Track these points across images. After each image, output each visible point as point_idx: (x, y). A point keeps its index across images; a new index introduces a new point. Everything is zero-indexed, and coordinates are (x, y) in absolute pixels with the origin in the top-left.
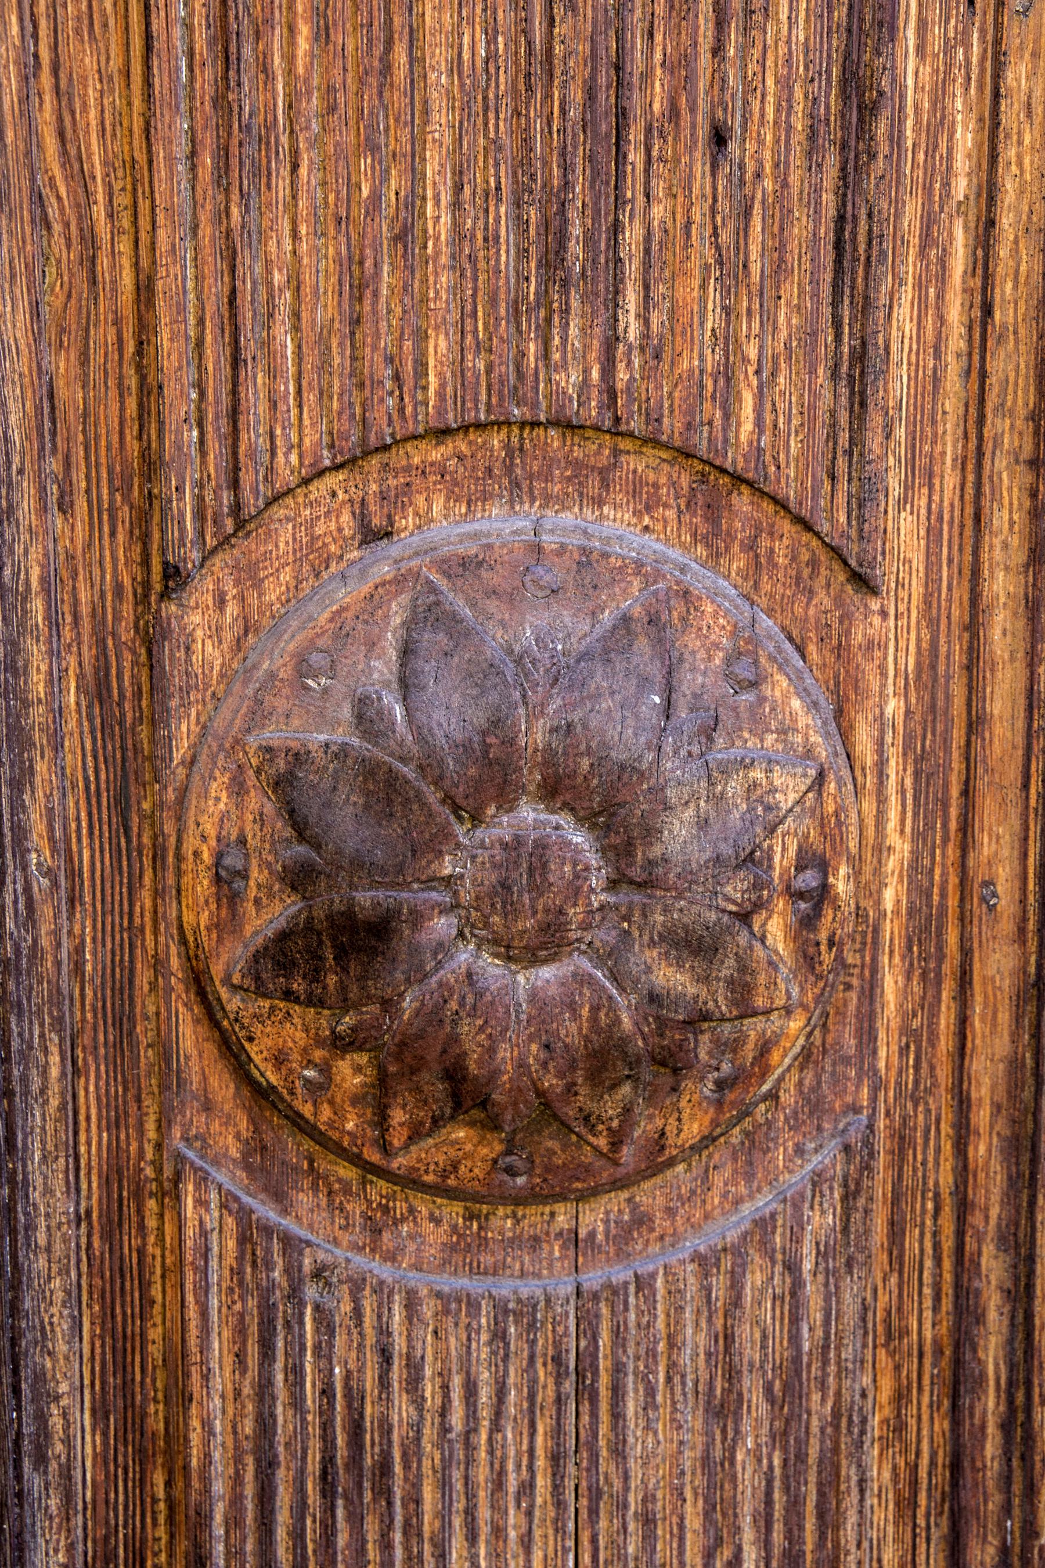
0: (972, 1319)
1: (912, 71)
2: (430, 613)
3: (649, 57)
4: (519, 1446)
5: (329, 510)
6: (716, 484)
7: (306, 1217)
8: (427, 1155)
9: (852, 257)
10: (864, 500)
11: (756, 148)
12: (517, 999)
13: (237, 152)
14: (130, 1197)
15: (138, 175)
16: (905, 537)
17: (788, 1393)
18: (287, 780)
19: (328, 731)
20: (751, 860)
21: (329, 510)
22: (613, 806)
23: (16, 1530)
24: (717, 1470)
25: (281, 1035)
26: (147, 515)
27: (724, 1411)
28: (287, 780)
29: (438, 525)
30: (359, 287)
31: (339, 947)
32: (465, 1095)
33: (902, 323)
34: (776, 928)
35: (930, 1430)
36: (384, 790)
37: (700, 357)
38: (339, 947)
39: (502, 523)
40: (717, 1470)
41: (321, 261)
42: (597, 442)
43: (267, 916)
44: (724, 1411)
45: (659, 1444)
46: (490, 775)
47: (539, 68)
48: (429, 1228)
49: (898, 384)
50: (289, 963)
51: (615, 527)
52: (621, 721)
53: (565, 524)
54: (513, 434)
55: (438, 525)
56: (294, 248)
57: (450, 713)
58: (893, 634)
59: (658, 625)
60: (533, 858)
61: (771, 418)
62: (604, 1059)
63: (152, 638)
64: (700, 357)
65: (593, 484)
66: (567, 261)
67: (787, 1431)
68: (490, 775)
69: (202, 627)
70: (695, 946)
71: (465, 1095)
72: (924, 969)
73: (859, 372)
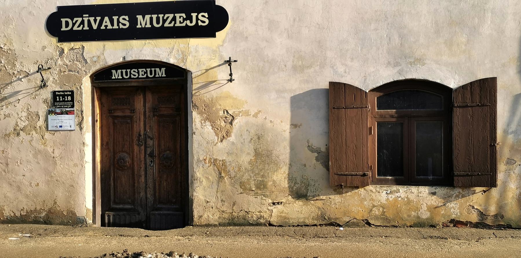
6: (127, 153)
46: (120, 159)
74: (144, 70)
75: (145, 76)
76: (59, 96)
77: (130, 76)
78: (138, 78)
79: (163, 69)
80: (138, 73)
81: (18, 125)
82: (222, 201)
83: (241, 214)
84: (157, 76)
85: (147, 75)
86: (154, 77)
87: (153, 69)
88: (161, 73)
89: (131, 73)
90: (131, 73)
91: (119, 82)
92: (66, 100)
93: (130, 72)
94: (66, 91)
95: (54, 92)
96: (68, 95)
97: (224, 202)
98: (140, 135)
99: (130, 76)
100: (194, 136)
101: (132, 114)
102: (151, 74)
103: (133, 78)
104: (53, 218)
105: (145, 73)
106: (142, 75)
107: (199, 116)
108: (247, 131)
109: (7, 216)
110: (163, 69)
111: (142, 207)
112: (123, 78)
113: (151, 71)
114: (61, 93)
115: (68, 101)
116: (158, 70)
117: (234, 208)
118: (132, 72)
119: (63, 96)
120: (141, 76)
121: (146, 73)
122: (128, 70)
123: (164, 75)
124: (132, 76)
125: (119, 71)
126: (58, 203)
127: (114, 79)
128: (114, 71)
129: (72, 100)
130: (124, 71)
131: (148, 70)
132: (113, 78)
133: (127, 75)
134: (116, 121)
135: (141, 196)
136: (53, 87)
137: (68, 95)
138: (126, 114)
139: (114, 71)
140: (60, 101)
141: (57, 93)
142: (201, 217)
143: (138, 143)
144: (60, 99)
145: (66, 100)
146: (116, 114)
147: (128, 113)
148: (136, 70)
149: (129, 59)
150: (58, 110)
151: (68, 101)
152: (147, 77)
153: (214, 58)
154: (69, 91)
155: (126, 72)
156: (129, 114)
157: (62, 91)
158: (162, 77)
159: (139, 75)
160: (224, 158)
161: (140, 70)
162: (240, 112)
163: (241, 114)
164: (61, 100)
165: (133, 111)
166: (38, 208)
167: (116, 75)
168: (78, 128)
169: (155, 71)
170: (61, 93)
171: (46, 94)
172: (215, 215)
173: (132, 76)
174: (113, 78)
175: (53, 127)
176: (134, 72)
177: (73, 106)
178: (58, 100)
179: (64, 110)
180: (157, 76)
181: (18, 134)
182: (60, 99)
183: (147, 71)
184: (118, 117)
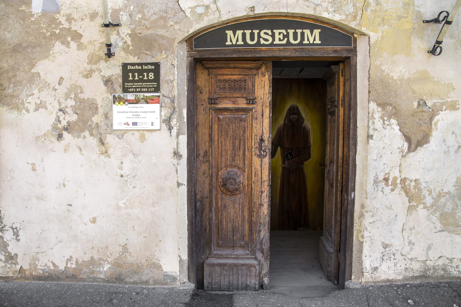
0: (198, 92)
1: (246, 153)
2: (228, 173)
3: (236, 153)
4: (231, 206)
5: (225, 169)
6: (239, 168)
7: (223, 196)
8: (228, 194)
9: (244, 160)
10: (245, 168)
11: (240, 156)
12: (231, 187)
13: (222, 156)
14: (217, 195)
15: (218, 157)
16: (246, 170)
17: (242, 204)
18: (223, 179)
19: (224, 177)
20: (240, 182)
21: (225, 169)
22: (235, 180)
23: (332, 164)
24: (239, 207)
25: (222, 189)
26: (218, 169)
27: (239, 205)
28: (223, 179)
29: (229, 169)
30: (226, 161)
31: (224, 185)
32: (229, 191)
33: (246, 162)
34: (241, 185)
35: (248, 206)
36: (226, 179)
37: (238, 163)
38: (224, 185)
39: (231, 169)
40: (239, 207)
41: (224, 160)
42: (235, 166)
43: (222, 184)
44: (239, 205)
45: (237, 206)
46: (230, 179)
47: (232, 153)
48: (228, 197)
49: (246, 165)
50: (222, 186)
51: (235, 170)
52: (235, 177)
53: (233, 169)
54: (232, 166)
55: (229, 169)
56: (223, 159)
57: (229, 176)
58: (246, 174)
59: (237, 173)
60: (232, 182)
61: (241, 166)
62: (234, 190)
63: (218, 173)
64: (238, 163)
65: (234, 168)
66: (233, 160)
67: (242, 205)
68: (230, 179)
69: (220, 173)
70: (238, 185)
71: (229, 191)
72: (248, 187)
73: (244, 164)
74: (284, 31)
75: (284, 42)
76: (133, 71)
77: (259, 41)
78: (272, 44)
79: (317, 32)
80: (273, 36)
81: (60, 122)
82: (410, 243)
83: (440, 262)
84: (306, 42)
85: (288, 40)
86: (301, 43)
87: (299, 31)
88: (313, 37)
89: (259, 37)
90: (259, 37)
91: (239, 51)
92: (146, 78)
93: (259, 34)
94: (146, 64)
95: (125, 66)
96: (148, 71)
97: (414, 244)
98: (262, 140)
99: (259, 41)
100: (371, 141)
101: (251, 106)
102: (295, 38)
103: (264, 45)
104: (1, 260)
105: (284, 36)
106: (280, 40)
107: (380, 109)
108: (453, 133)
109: (43, 270)
110: (317, 32)
111: (263, 253)
112: (246, 44)
113: (295, 35)
114: (137, 67)
115: (149, 81)
116: (307, 32)
117: (430, 252)
118: (262, 34)
119: (141, 72)
120: (277, 42)
121: (287, 36)
122: (256, 32)
123: (318, 41)
124: (262, 42)
125: (239, 33)
126: (130, 250)
127: (229, 46)
128: (229, 33)
129: (157, 79)
130: (248, 32)
131: (291, 32)
132: (228, 43)
133: (252, 39)
134: (221, 117)
135: (262, 236)
136: (121, 57)
137: (148, 71)
138: (240, 106)
139: (229, 33)
140: (134, 81)
141: (129, 67)
142: (376, 269)
143: (260, 152)
144: (134, 76)
145: (146, 78)
146: (220, 106)
147: (242, 104)
148: (269, 32)
149: (259, 11)
150: (130, 96)
151: (149, 81)
152: (288, 43)
153: (405, 15)
154: (152, 64)
155: (252, 35)
156: (245, 106)
157: (139, 64)
158: (313, 44)
159: (274, 40)
160: (418, 177)
161: (277, 32)
162: (443, 104)
163: (444, 107)
164: (137, 78)
165: (252, 101)
166: (96, 257)
167: (234, 38)
168: (164, 127)
169: (303, 34)
170: (137, 67)
171: (113, 69)
172: (398, 265)
173: (262, 42)
174: (228, 43)
175: (120, 124)
176: (265, 36)
177: (157, 89)
178: (131, 78)
179: (141, 95)
180: (306, 42)
181: (60, 137)
182: (134, 76)
183: (288, 33)
184: (226, 110)
